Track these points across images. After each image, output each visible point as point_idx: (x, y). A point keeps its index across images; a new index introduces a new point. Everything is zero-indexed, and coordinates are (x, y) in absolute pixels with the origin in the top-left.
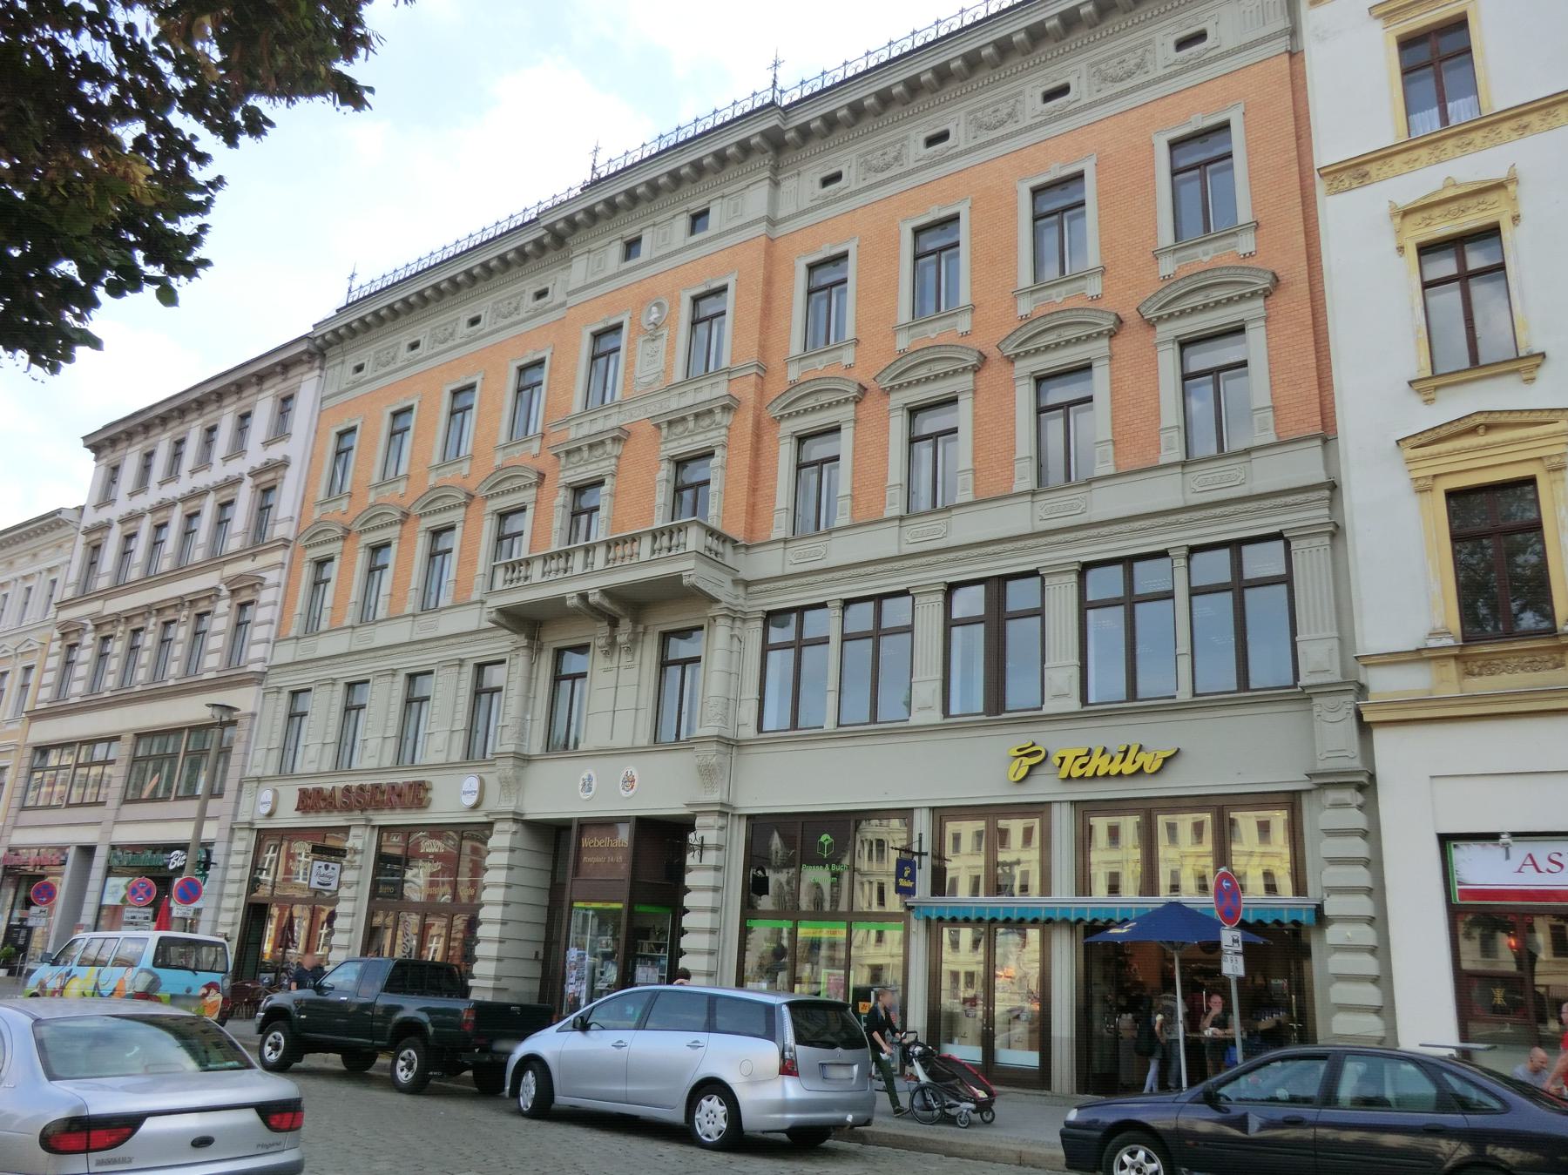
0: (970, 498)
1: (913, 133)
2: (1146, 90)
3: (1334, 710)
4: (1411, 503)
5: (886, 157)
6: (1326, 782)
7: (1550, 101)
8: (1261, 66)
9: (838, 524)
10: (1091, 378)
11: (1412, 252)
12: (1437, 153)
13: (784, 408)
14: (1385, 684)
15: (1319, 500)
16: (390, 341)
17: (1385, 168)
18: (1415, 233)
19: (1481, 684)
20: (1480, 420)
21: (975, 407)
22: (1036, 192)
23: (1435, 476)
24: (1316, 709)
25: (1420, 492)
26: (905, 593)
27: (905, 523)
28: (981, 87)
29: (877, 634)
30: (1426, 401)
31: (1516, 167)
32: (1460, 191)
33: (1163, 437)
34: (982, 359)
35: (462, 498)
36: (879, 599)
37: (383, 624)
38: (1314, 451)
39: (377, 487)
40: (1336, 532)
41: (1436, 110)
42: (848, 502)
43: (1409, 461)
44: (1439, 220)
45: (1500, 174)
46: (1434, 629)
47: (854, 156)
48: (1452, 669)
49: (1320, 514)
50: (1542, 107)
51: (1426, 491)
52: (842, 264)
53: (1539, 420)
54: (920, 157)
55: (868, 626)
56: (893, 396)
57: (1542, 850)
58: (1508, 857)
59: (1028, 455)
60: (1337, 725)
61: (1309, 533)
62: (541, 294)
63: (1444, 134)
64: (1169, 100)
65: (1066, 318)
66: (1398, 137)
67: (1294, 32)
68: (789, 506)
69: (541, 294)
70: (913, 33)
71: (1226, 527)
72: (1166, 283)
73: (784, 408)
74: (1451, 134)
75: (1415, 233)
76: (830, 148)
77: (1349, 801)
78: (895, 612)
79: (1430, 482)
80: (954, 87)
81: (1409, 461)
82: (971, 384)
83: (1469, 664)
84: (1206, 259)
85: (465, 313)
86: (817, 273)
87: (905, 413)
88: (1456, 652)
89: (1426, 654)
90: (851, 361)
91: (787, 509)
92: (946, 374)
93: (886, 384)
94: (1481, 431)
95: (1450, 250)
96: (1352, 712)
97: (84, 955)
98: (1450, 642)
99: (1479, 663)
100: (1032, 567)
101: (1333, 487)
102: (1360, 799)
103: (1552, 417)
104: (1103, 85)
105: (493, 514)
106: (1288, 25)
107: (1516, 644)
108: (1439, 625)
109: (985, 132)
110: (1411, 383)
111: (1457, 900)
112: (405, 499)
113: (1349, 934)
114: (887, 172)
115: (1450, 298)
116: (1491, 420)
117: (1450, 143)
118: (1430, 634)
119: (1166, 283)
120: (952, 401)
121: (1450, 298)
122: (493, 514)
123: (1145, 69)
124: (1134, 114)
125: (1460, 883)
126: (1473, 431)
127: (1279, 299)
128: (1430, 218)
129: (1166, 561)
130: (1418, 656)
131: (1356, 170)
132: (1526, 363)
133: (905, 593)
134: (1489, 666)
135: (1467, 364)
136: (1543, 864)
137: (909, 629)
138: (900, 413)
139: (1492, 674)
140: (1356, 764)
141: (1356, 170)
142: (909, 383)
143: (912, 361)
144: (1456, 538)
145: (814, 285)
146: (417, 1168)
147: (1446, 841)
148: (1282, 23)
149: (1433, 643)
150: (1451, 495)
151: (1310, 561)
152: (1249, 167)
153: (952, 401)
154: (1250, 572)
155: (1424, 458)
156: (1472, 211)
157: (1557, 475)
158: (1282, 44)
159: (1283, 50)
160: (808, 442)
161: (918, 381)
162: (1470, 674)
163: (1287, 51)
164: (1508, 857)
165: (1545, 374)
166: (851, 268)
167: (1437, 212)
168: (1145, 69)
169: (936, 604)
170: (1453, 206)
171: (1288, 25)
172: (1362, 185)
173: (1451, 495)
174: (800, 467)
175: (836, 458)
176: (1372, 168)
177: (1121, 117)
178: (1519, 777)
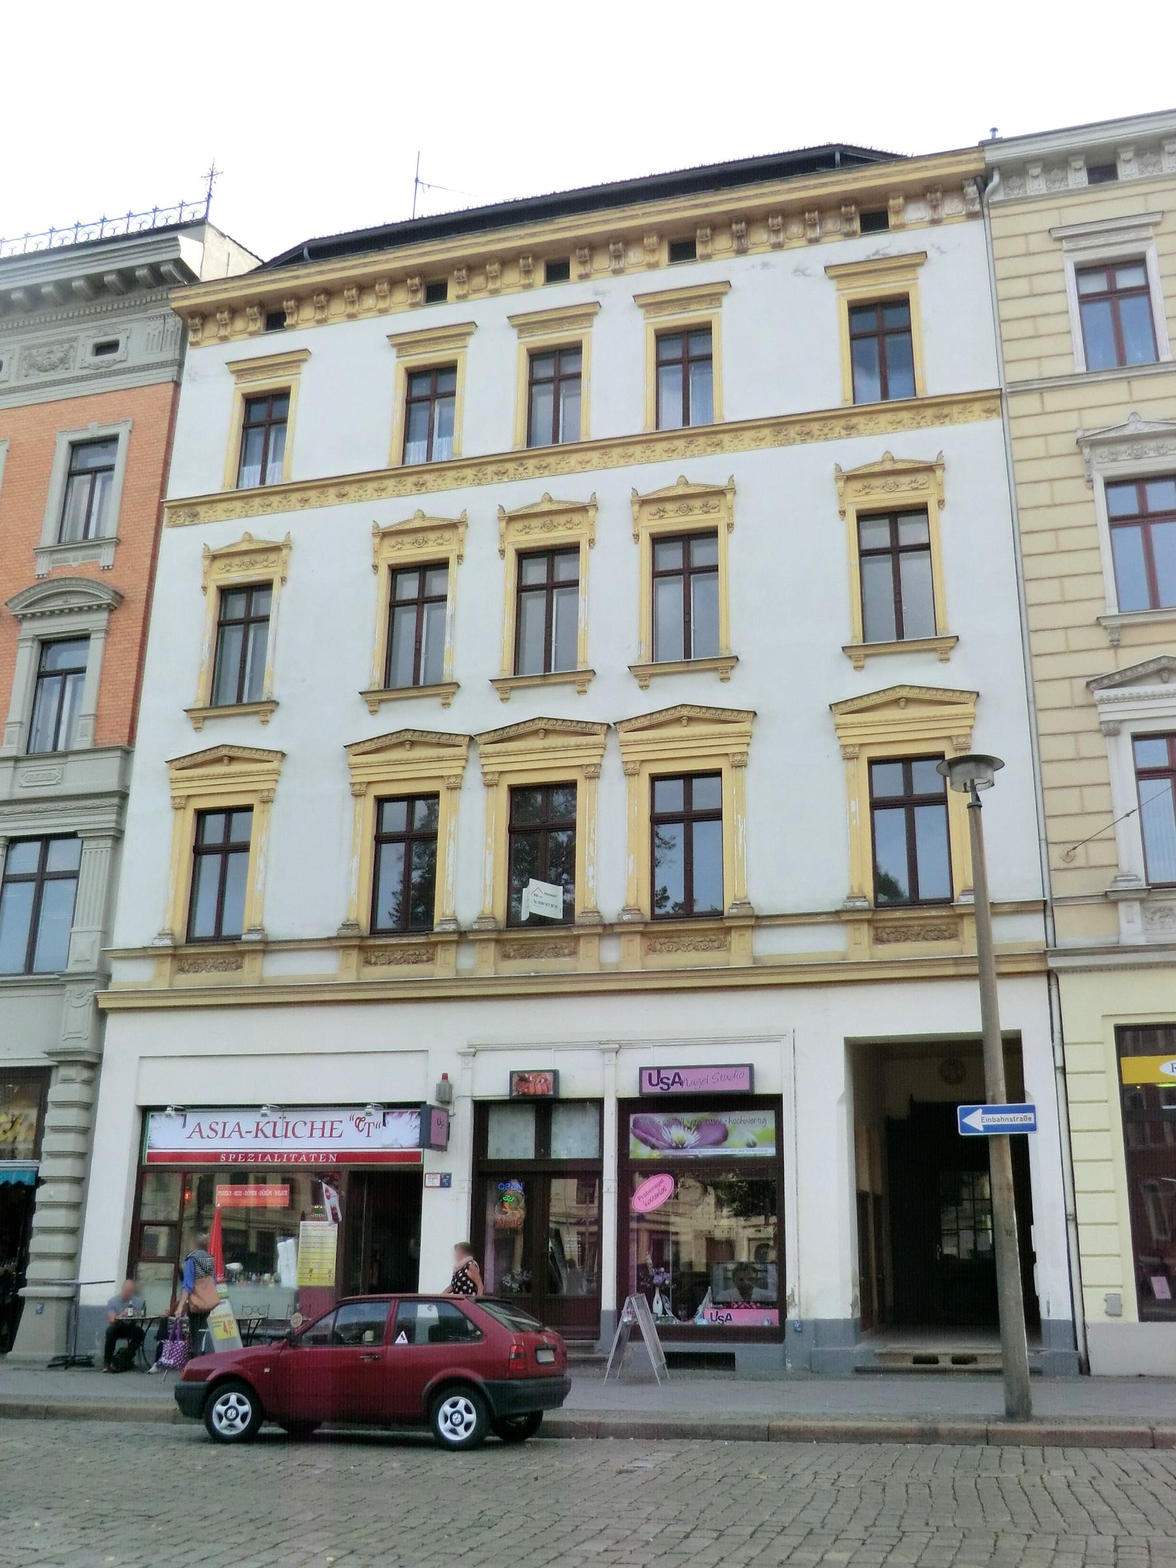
0: (86, 744)
1: (82, 335)
2: (60, 387)
3: (81, 996)
4: (168, 816)
5: (52, 356)
6: (67, 1059)
7: (337, 481)
8: (153, 389)
9: (76, 746)
10: (87, 648)
11: (646, 541)
12: (648, 452)
13: (27, 606)
14: (126, 975)
15: (110, 806)
16: (67, 331)
17: (872, 424)
18: (856, 499)
19: (187, 980)
20: (225, 752)
21: (105, 650)
22: (75, 446)
23: (861, 745)
24: (68, 994)
25: (848, 759)
26: (72, 835)
27: (21, 764)
28: (105, 312)
29: (41, 878)
30: (856, 668)
31: (597, 495)
32: (554, 507)
33: (7, 730)
34: (118, 597)
35: (107, 599)
36: (46, 840)
37: (81, 757)
38: (112, 762)
39: (52, 551)
40: (118, 837)
41: (260, 467)
42: (90, 722)
43: (173, 781)
44: (672, 514)
45: (583, 498)
46: (483, 912)
47: (17, 347)
48: (167, 966)
49: (107, 819)
50: (736, 430)
51: (853, 758)
52: (111, 447)
53: (730, 719)
54: (86, 364)
55: (32, 868)
56: (26, 625)
57: (206, 1119)
58: (184, 1126)
59: (19, 720)
60: (79, 1010)
61: (96, 835)
62: (103, 348)
63: (526, 454)
64: (77, 402)
65: (80, 586)
66: (515, 445)
67: (181, 365)
68: (25, 720)
69: (103, 348)
70: (103, 221)
71: (29, 824)
72: (40, 581)
73: (27, 606)
74: (435, 468)
75: (856, 499)
76: (18, 327)
77: (74, 1077)
78: (61, 857)
79: (364, 787)
80: (109, 299)
81: (173, 781)
82: (105, 623)
83: (508, 947)
84: (75, 564)
85: (90, 333)
86: (82, 453)
87: (36, 645)
88: (868, 916)
89: (845, 917)
90: (110, 563)
91: (21, 723)
92: (81, 609)
93: (19, 611)
94: (902, 704)
95: (678, 544)
96: (92, 999)
97: (640, 1262)
98: (866, 904)
99: (189, 962)
100: (71, 829)
101: (123, 796)
102: (85, 1074)
103: (962, 698)
104: (31, 372)
105: (33, 640)
106: (177, 357)
107: (678, 925)
108: (632, 902)
109: (36, 372)
110: (843, 648)
111: (145, 1162)
112: (109, 574)
113: (52, 1193)
114: (52, 372)
115: (882, 568)
116: (232, 753)
117: (660, 446)
118: (159, 935)
119: (40, 581)
120: (84, 638)
121: (672, 592)
122: (33, 640)
123: (67, 366)
124: (48, 408)
125: (150, 1148)
126: (219, 760)
127: (120, 615)
128: (663, 511)
129: (77, 842)
130: (838, 917)
131: (192, 508)
132: (725, 665)
133: (72, 835)
134: (902, 934)
135: (411, 685)
136: (206, 1131)
137: (73, 875)
138: (29, 644)
139: (196, 972)
140: (86, 1045)
141: (192, 508)
142: (43, 613)
143: (46, 590)
144: (513, 831)
145: (77, 466)
146: (136, 1544)
147: (146, 1112)
148: (170, 354)
149: (626, 918)
150: (514, 790)
151: (93, 861)
152: (124, 483)
153: (84, 638)
154: (53, 866)
155: (183, 780)
156: (560, 528)
157: (592, 781)
158: (169, 373)
159: (170, 379)
160: (55, 648)
161: (52, 613)
162: (182, 970)
163: (173, 381)
164: (184, 1126)
165: (276, 719)
166: (120, 456)
167: (236, 561)
168: (67, 366)
169: (104, 850)
170: (246, 559)
171: (177, 357)
172: (192, 524)
173: (514, 790)
174: (41, 675)
175: (81, 670)
176: (201, 510)
177: (36, 408)
178: (265, 1059)
